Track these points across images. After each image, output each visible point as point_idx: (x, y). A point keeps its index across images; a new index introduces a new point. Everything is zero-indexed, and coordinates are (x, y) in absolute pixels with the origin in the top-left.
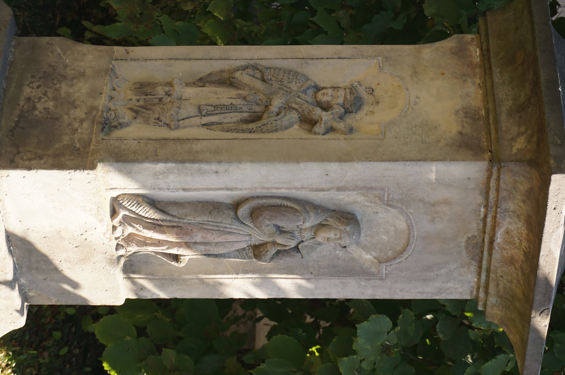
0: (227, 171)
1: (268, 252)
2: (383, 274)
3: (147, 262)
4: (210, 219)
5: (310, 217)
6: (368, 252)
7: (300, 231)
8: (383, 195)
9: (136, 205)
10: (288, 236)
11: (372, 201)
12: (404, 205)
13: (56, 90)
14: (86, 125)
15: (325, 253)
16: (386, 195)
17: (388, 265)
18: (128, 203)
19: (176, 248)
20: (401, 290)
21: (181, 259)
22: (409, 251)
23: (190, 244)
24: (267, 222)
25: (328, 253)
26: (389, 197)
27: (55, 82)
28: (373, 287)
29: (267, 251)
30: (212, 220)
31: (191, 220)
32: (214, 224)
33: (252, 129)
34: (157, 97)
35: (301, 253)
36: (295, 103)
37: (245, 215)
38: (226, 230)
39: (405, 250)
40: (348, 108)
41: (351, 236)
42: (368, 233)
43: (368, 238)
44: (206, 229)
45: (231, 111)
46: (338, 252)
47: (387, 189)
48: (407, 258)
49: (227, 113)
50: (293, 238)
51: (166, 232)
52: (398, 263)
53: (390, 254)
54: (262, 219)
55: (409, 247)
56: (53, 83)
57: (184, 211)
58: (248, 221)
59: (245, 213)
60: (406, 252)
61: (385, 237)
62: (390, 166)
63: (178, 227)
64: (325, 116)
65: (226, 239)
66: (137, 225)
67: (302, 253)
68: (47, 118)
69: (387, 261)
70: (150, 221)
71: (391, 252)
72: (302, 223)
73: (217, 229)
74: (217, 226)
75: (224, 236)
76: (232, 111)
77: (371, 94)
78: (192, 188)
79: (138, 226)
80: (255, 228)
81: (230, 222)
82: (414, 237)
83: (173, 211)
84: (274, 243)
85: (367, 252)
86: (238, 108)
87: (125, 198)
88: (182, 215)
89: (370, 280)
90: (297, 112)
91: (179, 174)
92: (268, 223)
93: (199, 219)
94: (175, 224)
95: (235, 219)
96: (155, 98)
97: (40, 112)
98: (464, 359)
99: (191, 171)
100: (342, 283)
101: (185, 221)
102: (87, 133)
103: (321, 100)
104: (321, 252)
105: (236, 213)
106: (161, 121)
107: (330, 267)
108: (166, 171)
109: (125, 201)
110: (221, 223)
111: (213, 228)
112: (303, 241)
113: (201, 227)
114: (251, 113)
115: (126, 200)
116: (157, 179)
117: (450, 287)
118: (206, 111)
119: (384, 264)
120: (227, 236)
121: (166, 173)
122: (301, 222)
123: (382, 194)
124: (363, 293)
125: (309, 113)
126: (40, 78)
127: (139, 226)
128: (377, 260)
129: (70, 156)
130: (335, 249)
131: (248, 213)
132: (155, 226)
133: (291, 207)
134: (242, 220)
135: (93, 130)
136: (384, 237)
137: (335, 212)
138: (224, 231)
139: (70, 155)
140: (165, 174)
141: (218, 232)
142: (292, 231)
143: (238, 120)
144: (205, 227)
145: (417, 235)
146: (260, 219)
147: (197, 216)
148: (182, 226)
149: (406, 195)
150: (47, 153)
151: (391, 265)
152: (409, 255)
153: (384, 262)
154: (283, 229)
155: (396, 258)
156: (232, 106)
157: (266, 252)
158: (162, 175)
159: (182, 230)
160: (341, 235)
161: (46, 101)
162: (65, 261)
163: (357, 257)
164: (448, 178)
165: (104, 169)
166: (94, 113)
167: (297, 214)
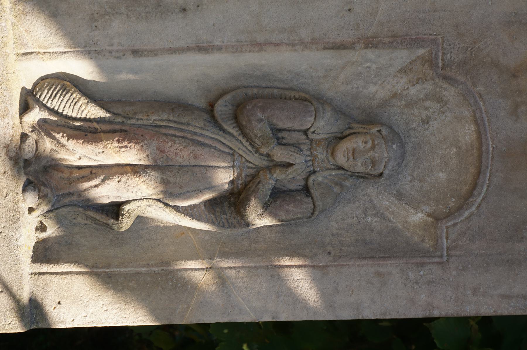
0: (200, 8)
1: (260, 185)
2: (443, 249)
3: (70, 244)
4: (171, 118)
7: (309, 146)
8: (436, 54)
9: (60, 93)
12: (469, 77)
15: (350, 221)
17: (451, 226)
18: (48, 93)
19: (117, 176)
21: (124, 209)
22: (482, 187)
24: (259, 114)
25: (355, 220)
28: (430, 282)
29: (259, 183)
30: (175, 119)
31: (142, 119)
41: (390, 144)
43: (416, 184)
44: (166, 135)
46: (369, 219)
48: (480, 204)
51: (103, 138)
52: (467, 218)
53: (452, 203)
54: (250, 107)
55: (481, 176)
58: (230, 124)
59: (226, 111)
61: (442, 176)
63: (121, 131)
66: (59, 133)
69: (450, 215)
70: (78, 124)
71: (453, 200)
73: (181, 134)
74: (182, 130)
75: (193, 148)
78: (145, 48)
79: (58, 136)
80: (240, 138)
81: (202, 125)
82: (488, 153)
85: (415, 209)
87: (44, 84)
88: (128, 113)
91: (127, 15)
92: (260, 115)
94: (117, 127)
99: (146, 7)
100: (378, 274)
101: (133, 121)
104: (343, 220)
107: (358, 244)
108: (109, 10)
109: (44, 91)
110: (188, 124)
111: (176, 133)
112: (314, 172)
115: (45, 88)
116: (94, 28)
120: (196, 149)
121: (108, 14)
122: (311, 116)
127: (63, 136)
130: (365, 214)
131: (230, 114)
134: (220, 120)
136: (441, 175)
138: (192, 140)
141: (184, 140)
142: (298, 144)
145: (493, 148)
147: (152, 113)
149: (471, 53)
151: (455, 224)
153: (444, 218)
154: (285, 141)
157: (256, 186)
160: (373, 142)
163: (400, 225)
165: (18, 8)
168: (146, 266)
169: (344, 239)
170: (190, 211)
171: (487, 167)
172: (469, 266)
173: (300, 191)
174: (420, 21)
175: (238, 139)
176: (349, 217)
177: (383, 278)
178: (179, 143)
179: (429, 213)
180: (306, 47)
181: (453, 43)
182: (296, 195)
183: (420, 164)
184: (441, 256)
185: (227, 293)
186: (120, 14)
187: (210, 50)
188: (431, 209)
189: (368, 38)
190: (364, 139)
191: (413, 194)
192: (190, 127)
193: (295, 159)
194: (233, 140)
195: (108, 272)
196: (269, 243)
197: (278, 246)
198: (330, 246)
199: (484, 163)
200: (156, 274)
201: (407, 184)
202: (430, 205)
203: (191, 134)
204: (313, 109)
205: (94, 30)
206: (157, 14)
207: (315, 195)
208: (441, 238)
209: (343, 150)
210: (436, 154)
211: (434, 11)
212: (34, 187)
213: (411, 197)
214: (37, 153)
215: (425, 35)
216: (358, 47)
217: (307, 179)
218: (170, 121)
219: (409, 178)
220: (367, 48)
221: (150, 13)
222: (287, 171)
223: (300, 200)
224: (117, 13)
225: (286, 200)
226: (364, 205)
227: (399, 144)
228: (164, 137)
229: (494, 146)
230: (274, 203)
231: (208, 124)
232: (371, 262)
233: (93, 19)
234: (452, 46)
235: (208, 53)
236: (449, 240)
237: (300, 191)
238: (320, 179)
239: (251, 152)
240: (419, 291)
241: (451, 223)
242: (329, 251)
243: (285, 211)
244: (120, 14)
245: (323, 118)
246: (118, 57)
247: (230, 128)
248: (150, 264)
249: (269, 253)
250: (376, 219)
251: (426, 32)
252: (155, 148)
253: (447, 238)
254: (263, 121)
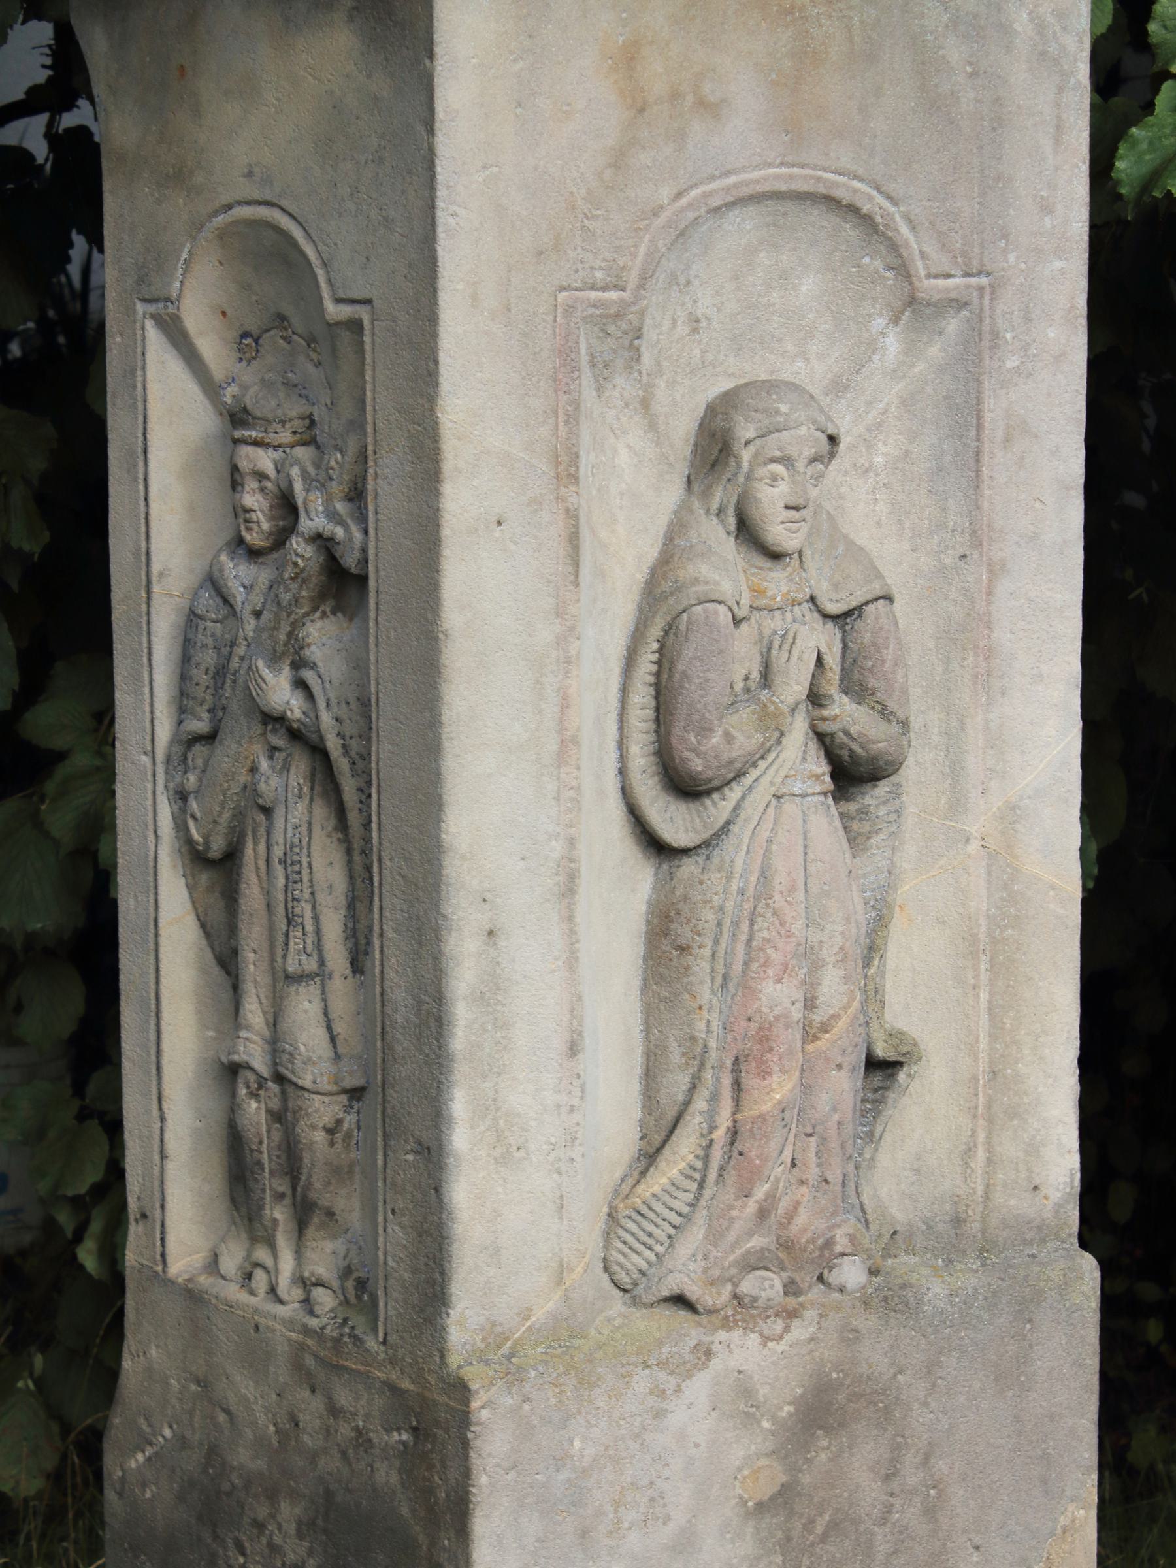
0: (489, 896)
2: (968, 287)
4: (707, 952)
5: (697, 581)
6: (872, 347)
8: (594, 306)
10: (779, 657)
11: (626, 343)
13: (247, 1485)
14: (344, 1398)
16: (593, 295)
17: (926, 267)
20: (1046, 208)
22: (855, 191)
23: (816, 1025)
24: (714, 740)
26: (600, 284)
27: (226, 1486)
28: (1027, 319)
29: (847, 733)
30: (710, 943)
31: (708, 1021)
32: (726, 934)
33: (362, 791)
34: (264, 1129)
35: (867, 603)
36: (275, 629)
37: (692, 821)
38: (750, 892)
39: (853, 210)
40: (294, 433)
42: (790, 347)
45: (305, 864)
46: (879, 460)
47: (564, 294)
48: (889, 197)
49: (311, 881)
50: (791, 640)
52: (913, 228)
55: (838, 193)
56: (229, 1494)
57: (673, 1045)
59: (684, 819)
60: (859, 204)
62: (460, 286)
64: (314, 520)
65: (792, 889)
67: (862, 600)
68: (325, 1531)
69: (903, 271)
72: (722, 609)
73: (745, 926)
74: (736, 923)
76: (305, 861)
77: (257, 343)
82: (791, 177)
83: (676, 1084)
84: (815, 698)
86: (296, 841)
89: (995, 334)
90: (304, 624)
91: (499, 1074)
93: (705, 994)
94: (727, 1080)
95: (708, 858)
96: (268, 1138)
97: (311, 1552)
98: (8, 336)
100: (1007, 440)
101: (713, 1044)
102: (366, 1396)
103: (270, 534)
105: (685, 851)
106: (339, 1122)
111: (743, 938)
112: (812, 599)
113: (738, 985)
114: (315, 792)
116: (522, 1154)
117: (1032, 20)
118: (304, 957)
119: (917, 284)
120: (778, 888)
122: (716, 613)
123: (591, 311)
124: (1059, 358)
125: (304, 581)
126: (216, 1537)
128: (902, 313)
129: (434, 1466)
131: (688, 808)
132: (735, 1154)
133: (660, 651)
135: (358, 1371)
136: (804, 288)
137: (692, 477)
139: (431, 1467)
140: (502, 1122)
143: (339, 839)
144: (737, 968)
145: (782, 164)
146: (700, 769)
148: (735, 1052)
150: (424, 1548)
151: (923, 255)
152: (878, 189)
153: (911, 283)
154: (755, 675)
155: (890, 239)
156: (289, 861)
158: (507, 1133)
159: (748, 1055)
160: (774, 460)
161: (280, 1528)
162: (887, 1478)
164: (515, 61)
166: (309, 1361)
167: (683, 627)
168: (977, 990)
169: (926, 522)
170: (868, 894)
171: (819, 179)
172: (1000, 222)
173: (845, 631)
174: (527, 345)
175: (750, 789)
176: (874, 510)
177: (1014, 429)
178: (769, 930)
179: (890, 320)
180: (572, 629)
181: (574, 263)
182: (858, 641)
183: (773, 336)
184: (981, 289)
185: (1030, 798)
186: (496, 1092)
187: (572, 865)
188: (881, 312)
189: (557, 476)
190: (766, 483)
191: (837, 354)
192: (727, 905)
193: (810, 650)
194: (751, 799)
195: (983, 1078)
196: (930, 701)
197: (938, 679)
198: (942, 556)
199: (804, 187)
200: (992, 966)
201: (812, 369)
202: (870, 315)
203: (742, 901)
204: (699, 608)
205: (528, 1154)
206: (499, 1001)
207: (861, 596)
208: (947, 290)
209: (784, 531)
210: (760, 299)
211: (509, 310)
212: (831, 1269)
213: (845, 359)
214: (298, 1198)
215: (554, 334)
216: (574, 500)
217: (826, 616)
218: (713, 955)
219: (799, 364)
220: (578, 478)
221: (496, 1019)
222: (831, 668)
223: (872, 632)
224: (495, 1100)
225: (873, 666)
226: (846, 473)
227: (774, 396)
228: (755, 966)
229: (778, 161)
230: (879, 694)
231: (716, 861)
232: (985, 459)
233: (505, 1160)
234: (580, 266)
235: (579, 872)
236: (953, 272)
237: (845, 631)
238: (825, 585)
239: (777, 756)
240: (1041, 343)
241: (919, 264)
242: (957, 560)
243: (896, 668)
244: (496, 1092)
245: (717, 584)
246: (583, 1091)
247: (719, 808)
248: (972, 981)
249: (958, 701)
250: (880, 444)
251: (549, 332)
252: (779, 986)
253: (948, 276)
254: (726, 729)
